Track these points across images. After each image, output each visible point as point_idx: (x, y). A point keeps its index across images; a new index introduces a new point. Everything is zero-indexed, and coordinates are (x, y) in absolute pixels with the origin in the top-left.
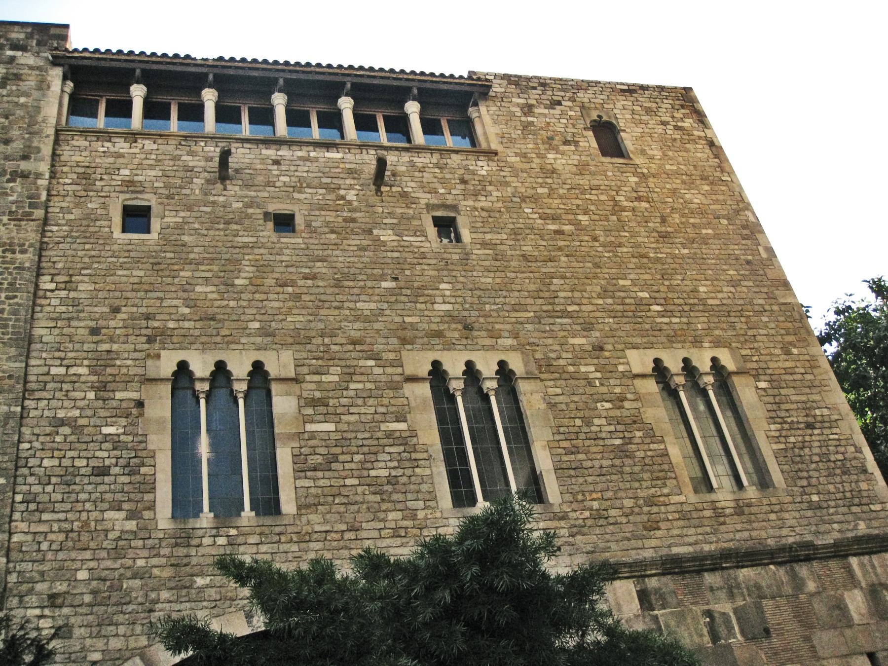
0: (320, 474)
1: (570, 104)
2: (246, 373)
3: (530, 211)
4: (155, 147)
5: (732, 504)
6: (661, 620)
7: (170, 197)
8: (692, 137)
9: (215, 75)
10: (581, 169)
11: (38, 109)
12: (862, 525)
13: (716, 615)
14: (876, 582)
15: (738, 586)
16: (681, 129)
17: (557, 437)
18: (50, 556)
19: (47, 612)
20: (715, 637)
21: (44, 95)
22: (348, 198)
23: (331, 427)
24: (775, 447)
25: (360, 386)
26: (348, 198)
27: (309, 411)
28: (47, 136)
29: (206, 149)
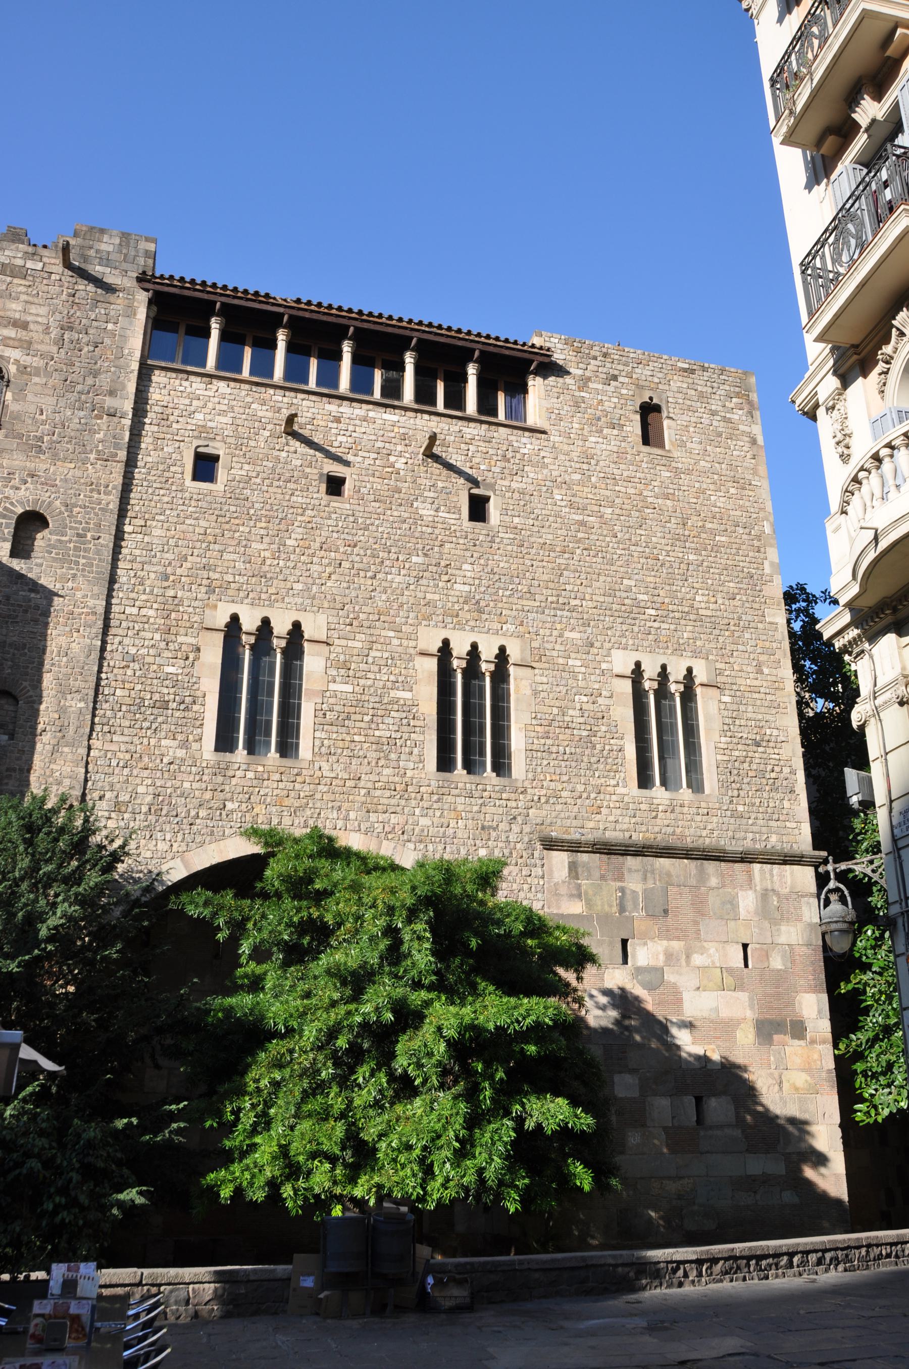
0: (335, 729)
1: (626, 380)
2: (286, 632)
3: (560, 497)
4: (229, 391)
5: (668, 802)
6: (583, 888)
7: (239, 447)
8: (736, 432)
9: (291, 317)
10: (621, 454)
11: (124, 337)
12: (774, 839)
13: (628, 892)
14: (769, 887)
15: (653, 872)
16: (729, 421)
17: (534, 722)
18: (117, 771)
19: (113, 815)
20: (622, 909)
21: (131, 323)
22: (397, 466)
23: (349, 688)
24: (719, 757)
25: (379, 654)
26: (397, 466)
27: (333, 672)
28: (132, 372)
29: (274, 398)
